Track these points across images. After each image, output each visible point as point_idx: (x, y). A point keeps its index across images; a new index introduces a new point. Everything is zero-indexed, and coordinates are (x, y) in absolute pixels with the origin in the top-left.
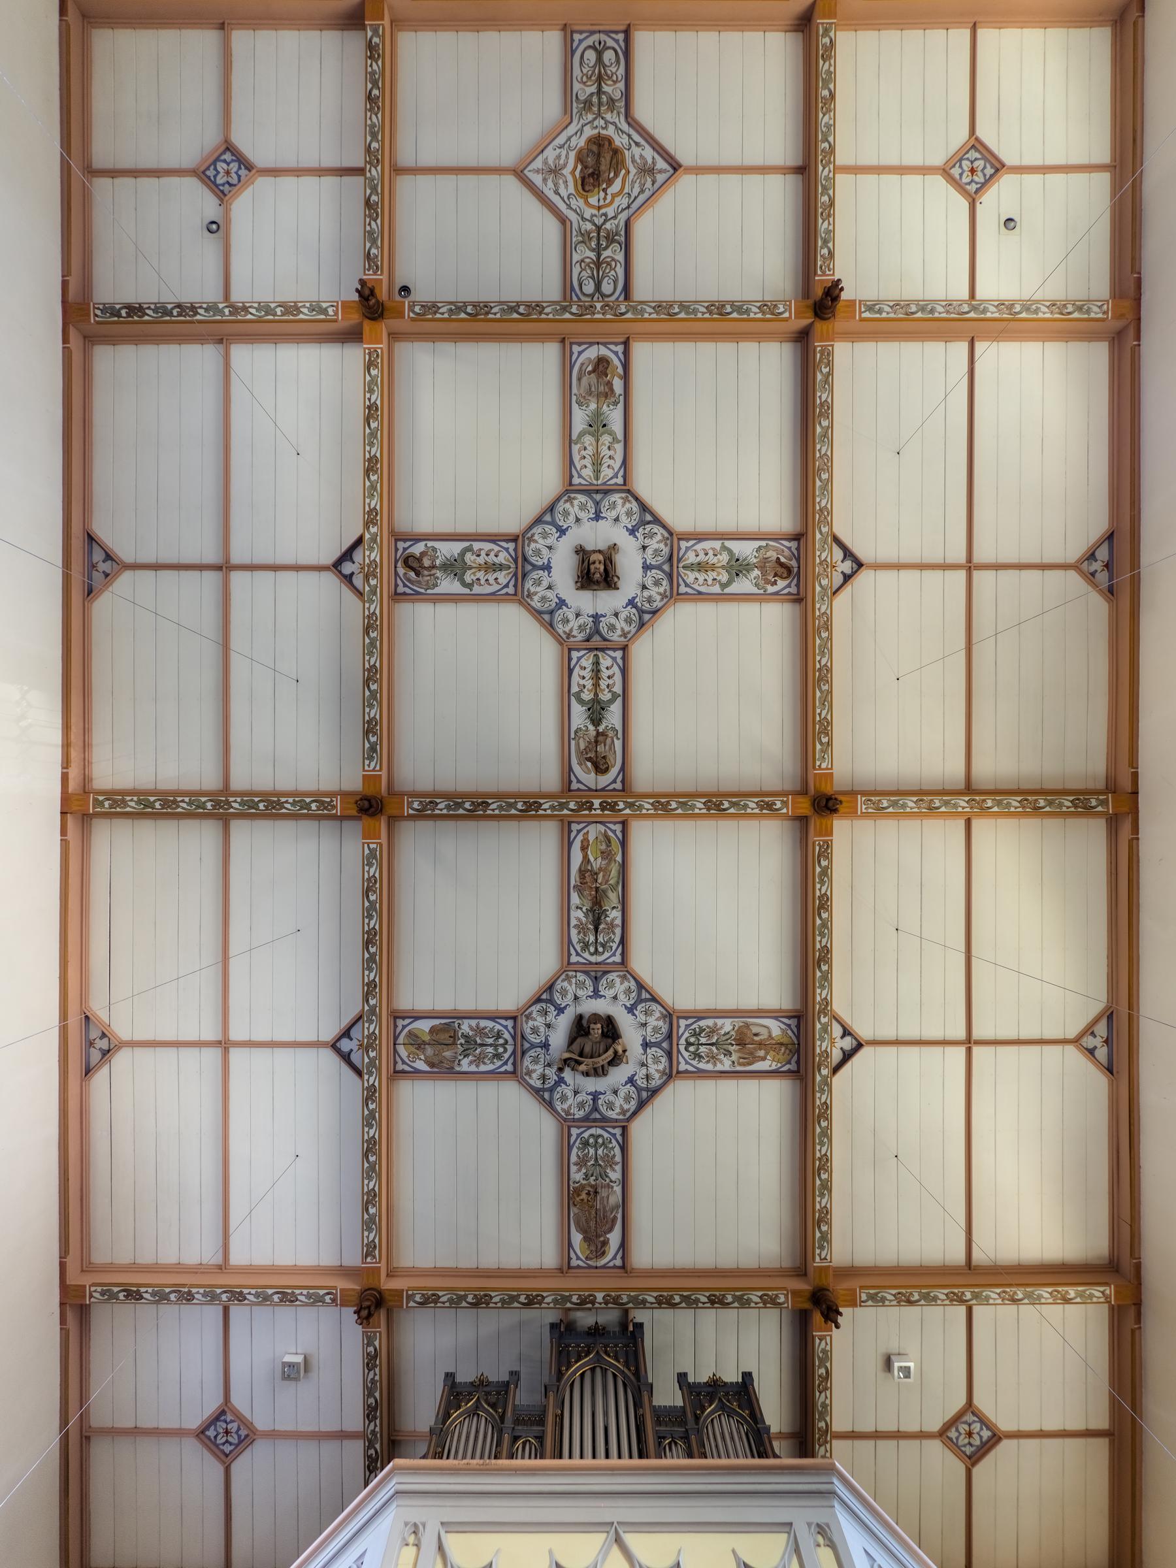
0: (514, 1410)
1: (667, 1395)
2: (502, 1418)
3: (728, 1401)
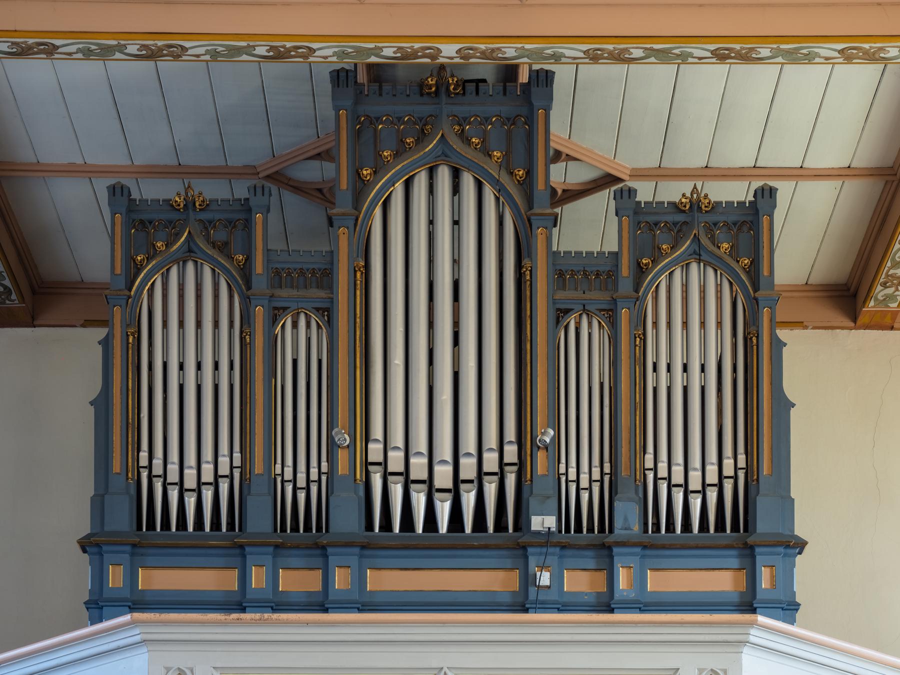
0: (268, 261)
1: (589, 229)
2: (246, 271)
3: (712, 239)
